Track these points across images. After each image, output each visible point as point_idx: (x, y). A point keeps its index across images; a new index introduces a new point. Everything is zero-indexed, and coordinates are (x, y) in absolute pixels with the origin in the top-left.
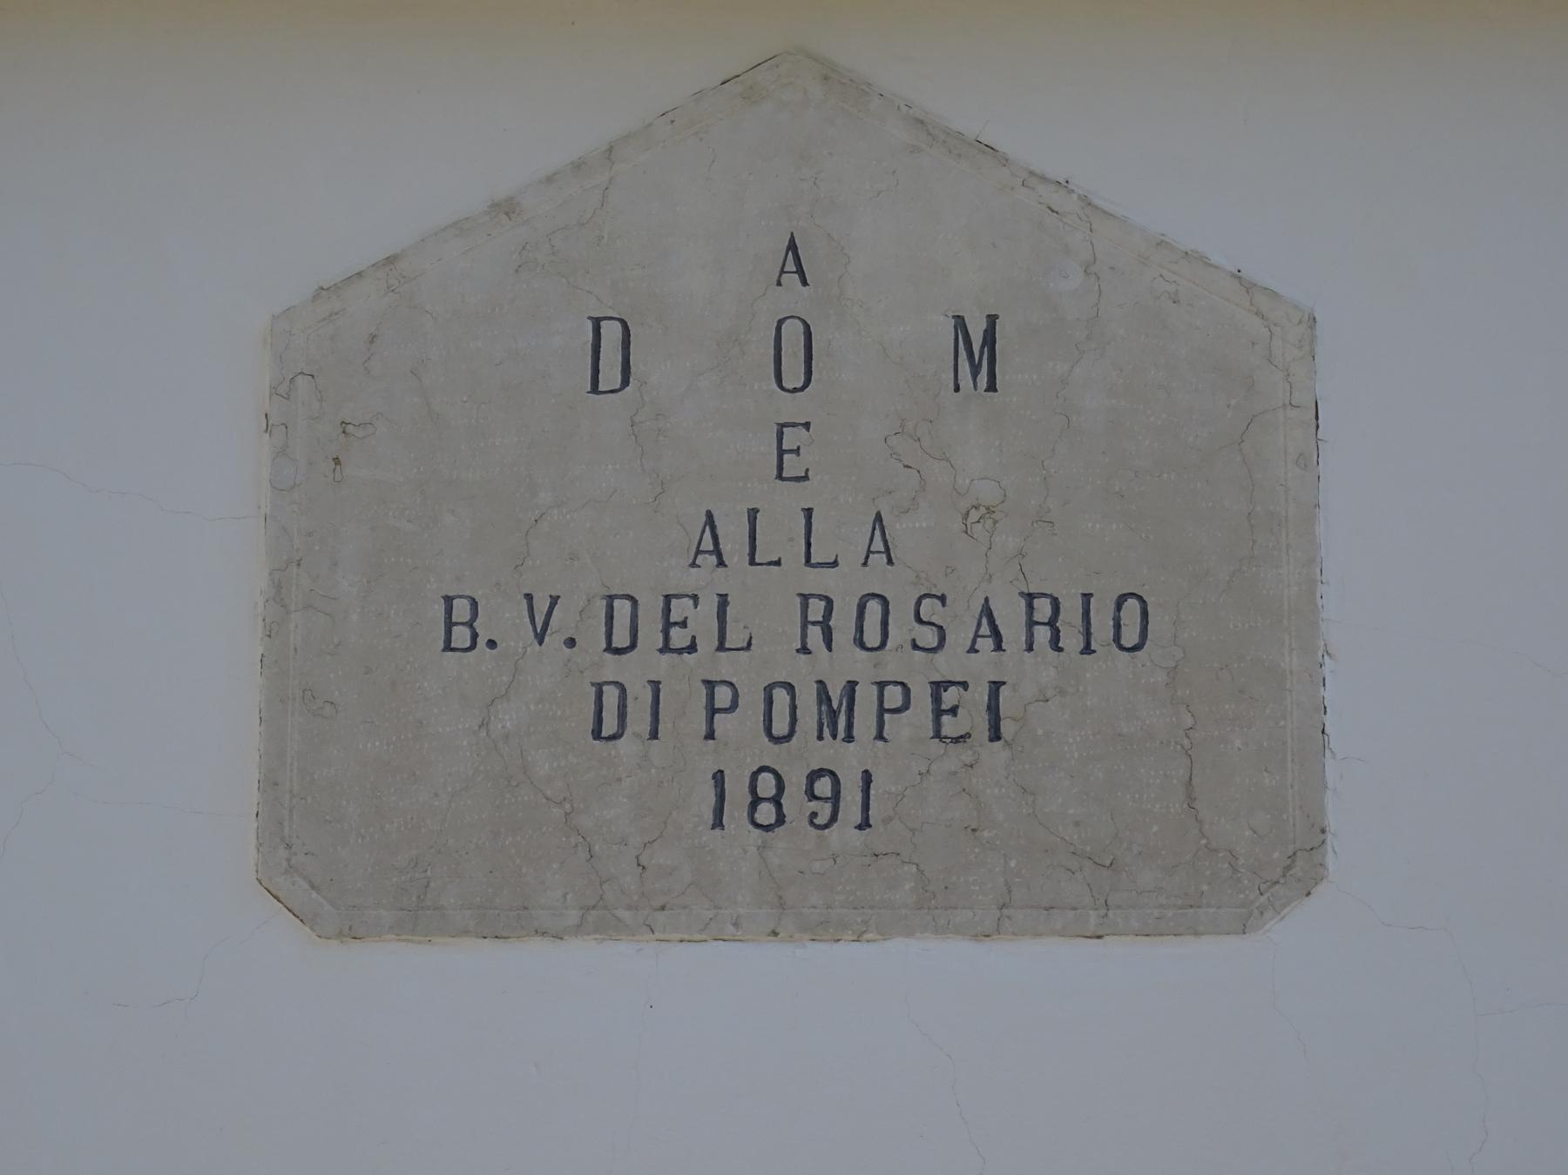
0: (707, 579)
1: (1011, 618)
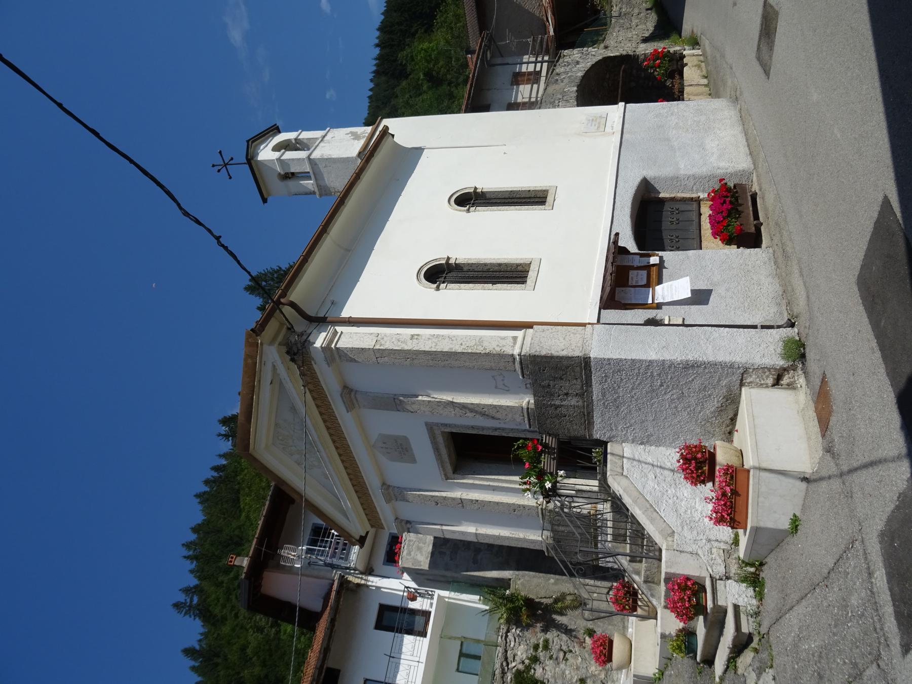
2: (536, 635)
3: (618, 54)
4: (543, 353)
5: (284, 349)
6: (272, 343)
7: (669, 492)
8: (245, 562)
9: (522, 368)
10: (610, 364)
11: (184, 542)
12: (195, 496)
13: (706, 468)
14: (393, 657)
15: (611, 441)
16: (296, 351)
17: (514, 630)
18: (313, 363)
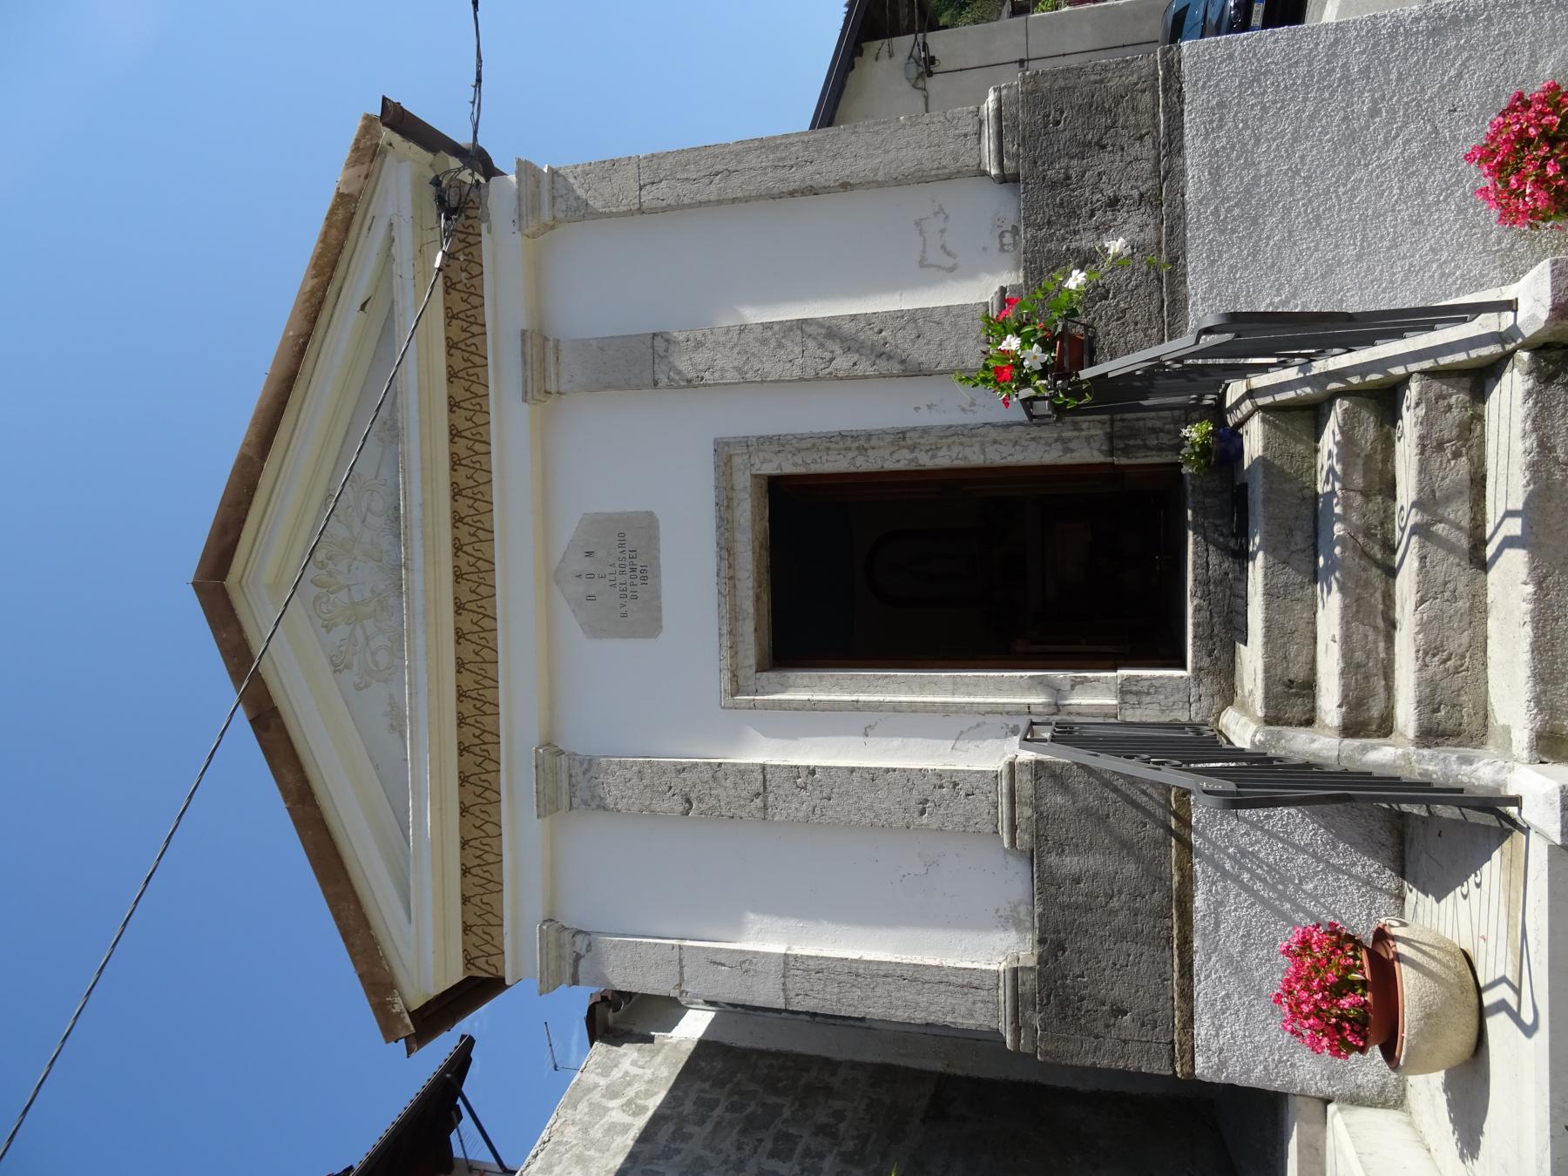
0: (618, 586)
1: (621, 549)
10: (1231, 56)
18: (484, 227)
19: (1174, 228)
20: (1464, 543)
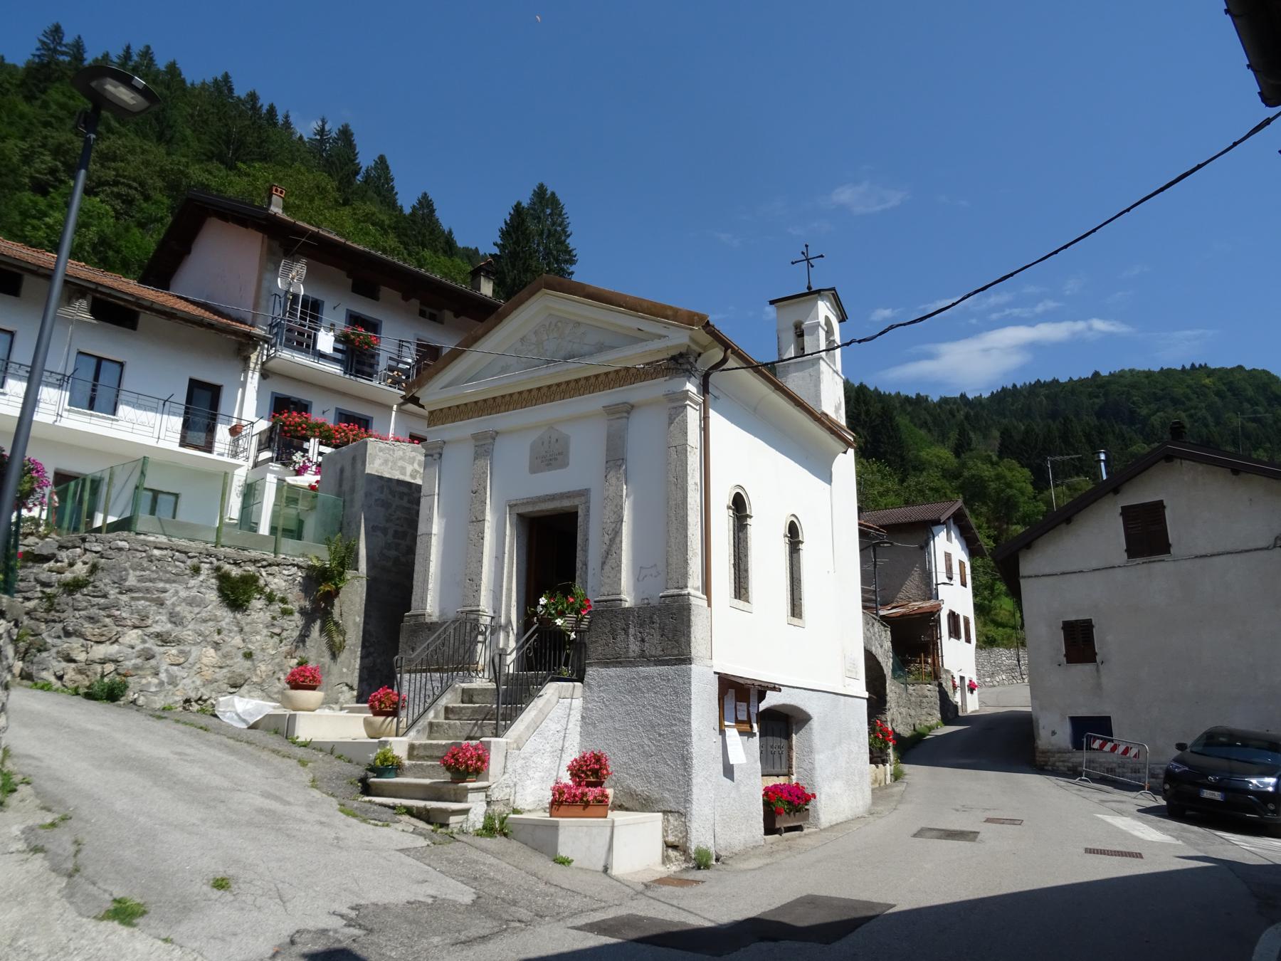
2: (297, 600)
3: (888, 691)
4: (693, 618)
5: (683, 350)
6: (692, 339)
7: (548, 746)
8: (276, 209)
9: (672, 596)
10: (684, 683)
11: (153, 49)
12: (226, 73)
13: (592, 779)
14: (164, 405)
15: (584, 686)
16: (680, 361)
17: (300, 574)
18: (667, 378)
19: (632, 663)
20: (472, 735)
